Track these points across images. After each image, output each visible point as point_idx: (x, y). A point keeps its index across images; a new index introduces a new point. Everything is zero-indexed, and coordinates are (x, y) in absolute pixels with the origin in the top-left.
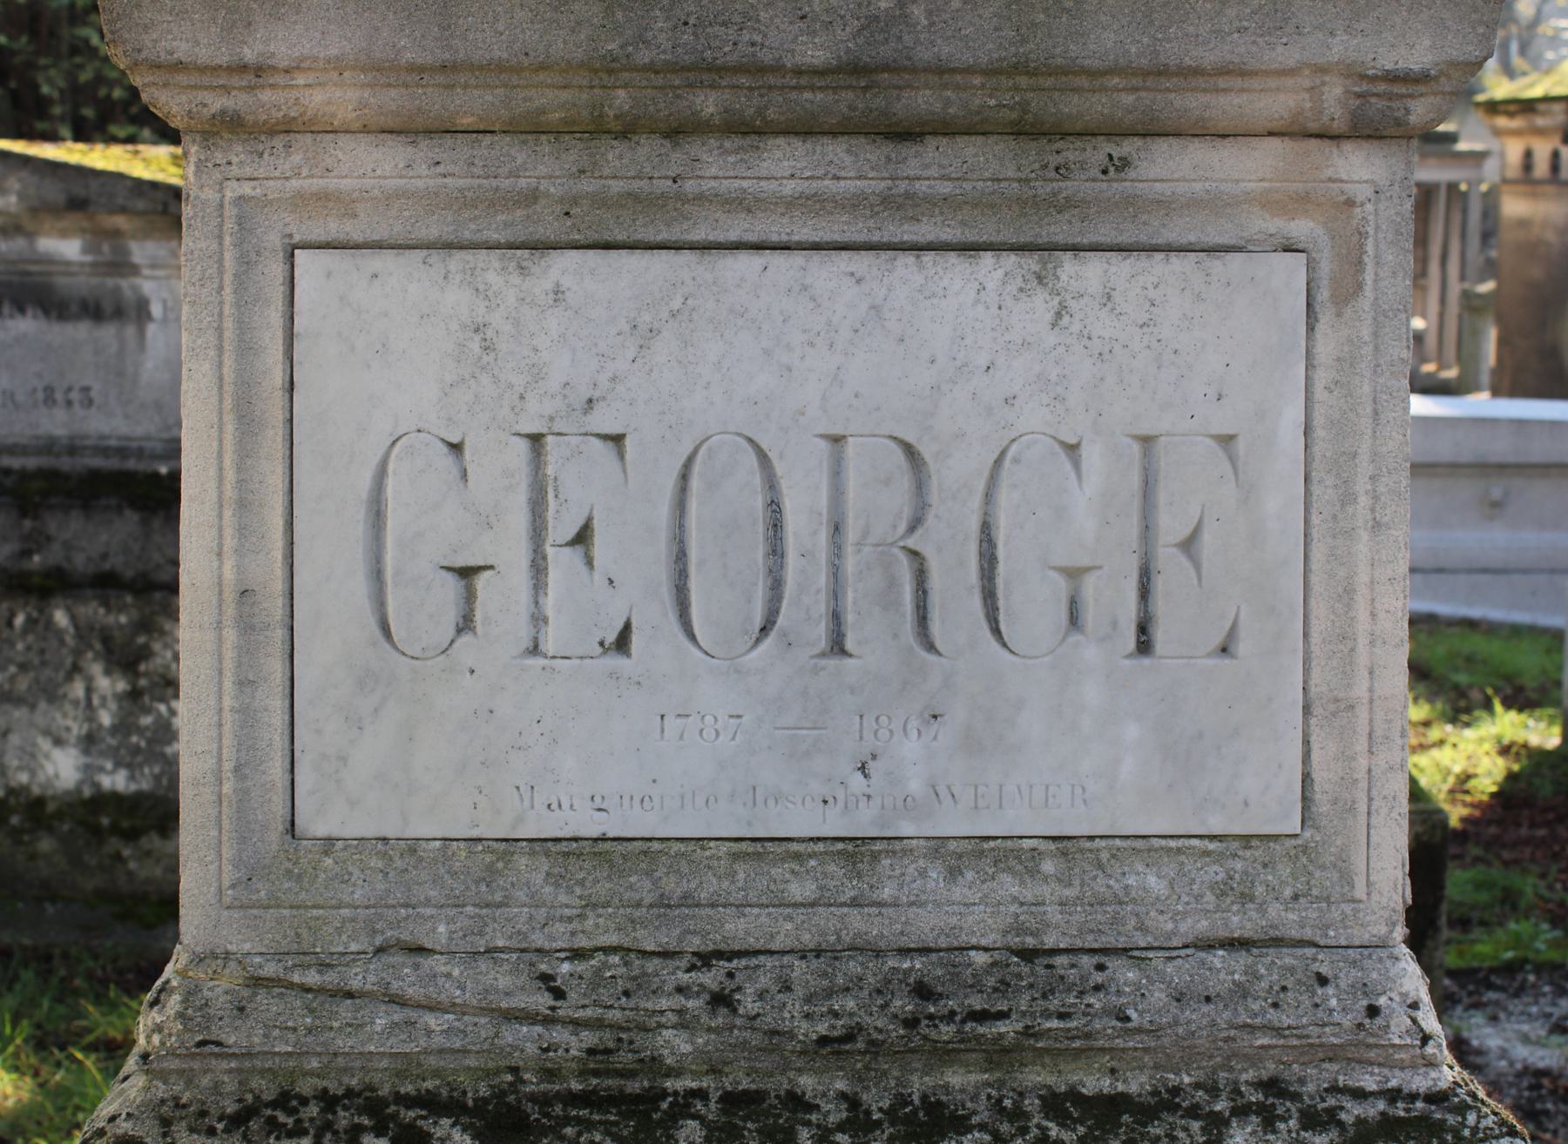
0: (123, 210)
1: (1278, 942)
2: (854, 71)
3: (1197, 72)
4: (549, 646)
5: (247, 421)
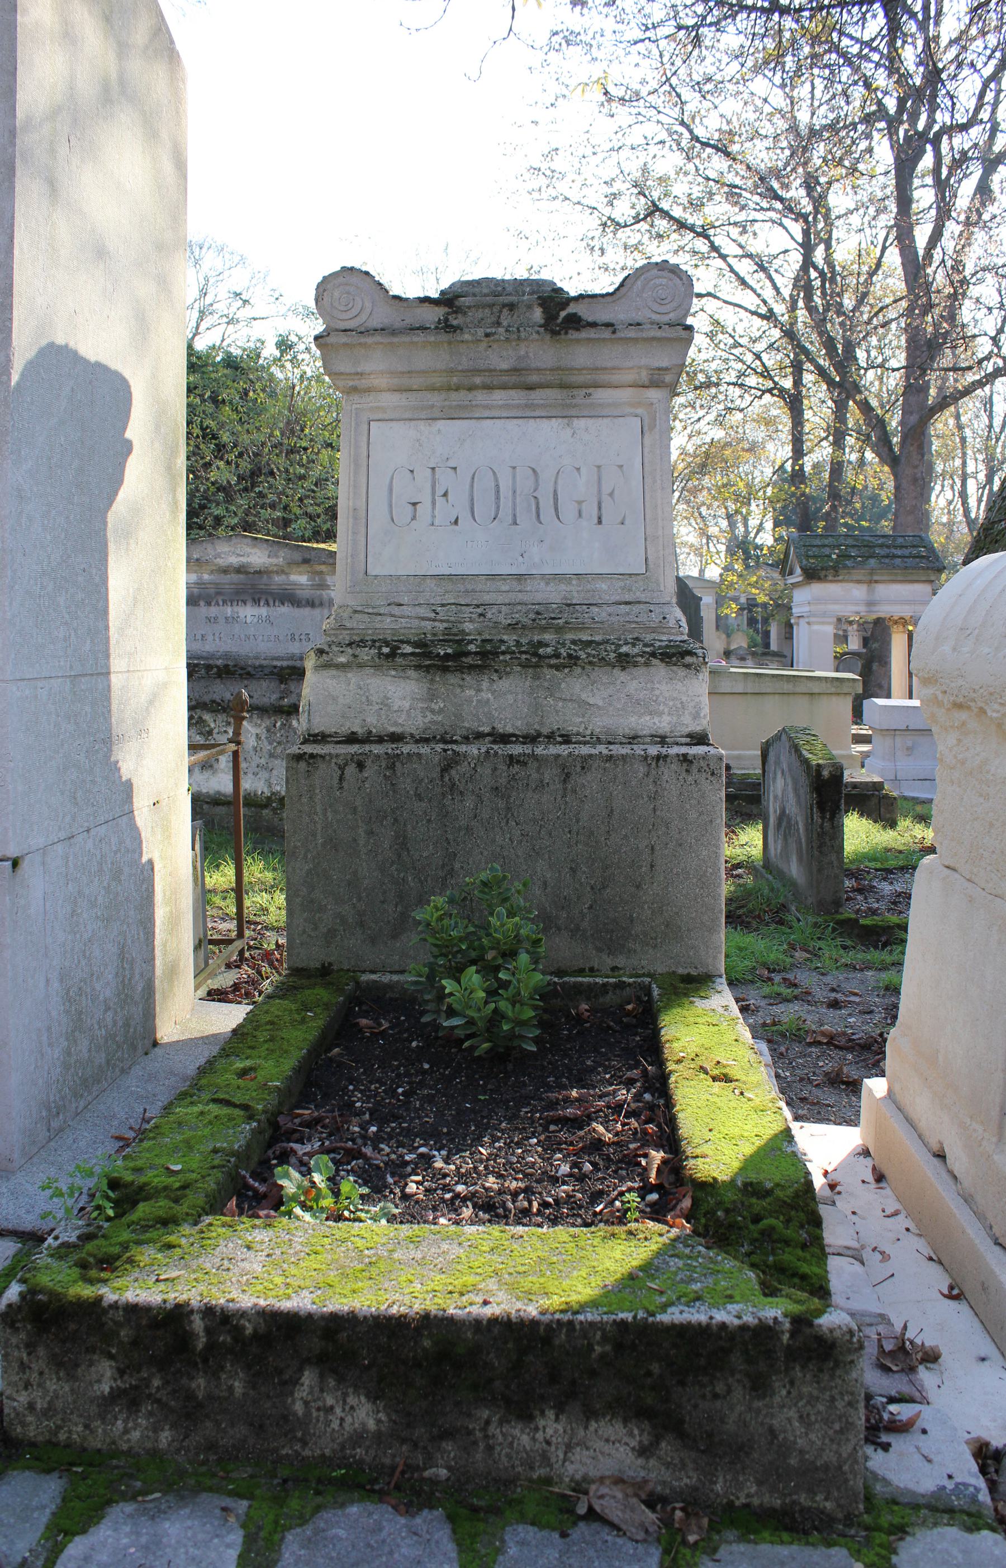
0: (324, 563)
1: (639, 602)
2: (515, 370)
3: (606, 369)
4: (436, 523)
5: (357, 465)
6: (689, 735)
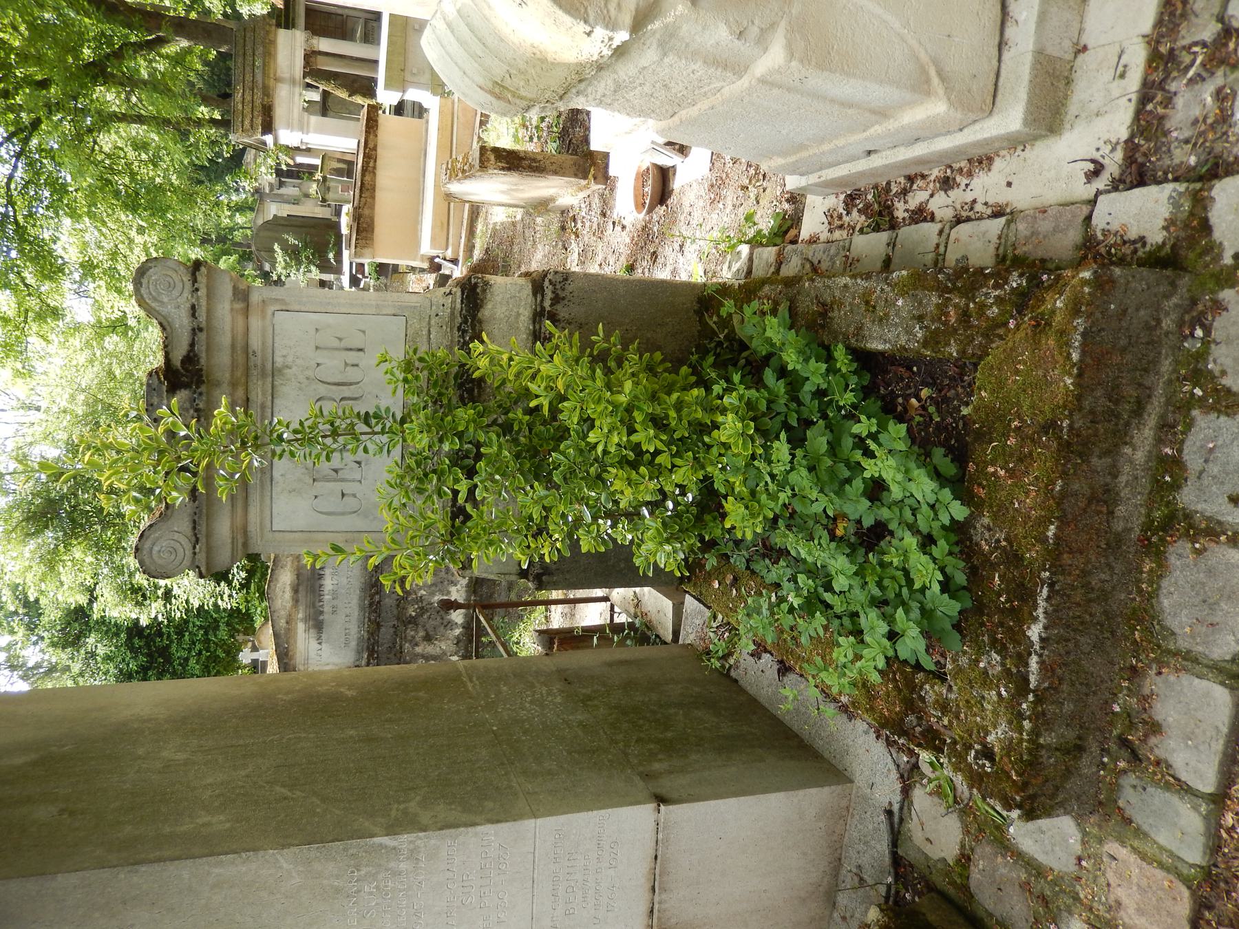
6: (535, 294)
